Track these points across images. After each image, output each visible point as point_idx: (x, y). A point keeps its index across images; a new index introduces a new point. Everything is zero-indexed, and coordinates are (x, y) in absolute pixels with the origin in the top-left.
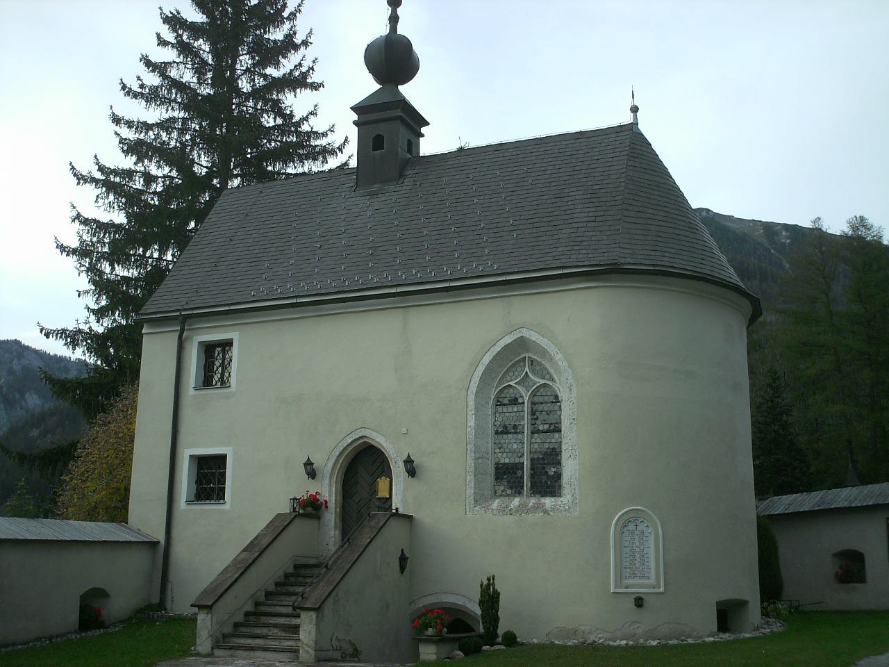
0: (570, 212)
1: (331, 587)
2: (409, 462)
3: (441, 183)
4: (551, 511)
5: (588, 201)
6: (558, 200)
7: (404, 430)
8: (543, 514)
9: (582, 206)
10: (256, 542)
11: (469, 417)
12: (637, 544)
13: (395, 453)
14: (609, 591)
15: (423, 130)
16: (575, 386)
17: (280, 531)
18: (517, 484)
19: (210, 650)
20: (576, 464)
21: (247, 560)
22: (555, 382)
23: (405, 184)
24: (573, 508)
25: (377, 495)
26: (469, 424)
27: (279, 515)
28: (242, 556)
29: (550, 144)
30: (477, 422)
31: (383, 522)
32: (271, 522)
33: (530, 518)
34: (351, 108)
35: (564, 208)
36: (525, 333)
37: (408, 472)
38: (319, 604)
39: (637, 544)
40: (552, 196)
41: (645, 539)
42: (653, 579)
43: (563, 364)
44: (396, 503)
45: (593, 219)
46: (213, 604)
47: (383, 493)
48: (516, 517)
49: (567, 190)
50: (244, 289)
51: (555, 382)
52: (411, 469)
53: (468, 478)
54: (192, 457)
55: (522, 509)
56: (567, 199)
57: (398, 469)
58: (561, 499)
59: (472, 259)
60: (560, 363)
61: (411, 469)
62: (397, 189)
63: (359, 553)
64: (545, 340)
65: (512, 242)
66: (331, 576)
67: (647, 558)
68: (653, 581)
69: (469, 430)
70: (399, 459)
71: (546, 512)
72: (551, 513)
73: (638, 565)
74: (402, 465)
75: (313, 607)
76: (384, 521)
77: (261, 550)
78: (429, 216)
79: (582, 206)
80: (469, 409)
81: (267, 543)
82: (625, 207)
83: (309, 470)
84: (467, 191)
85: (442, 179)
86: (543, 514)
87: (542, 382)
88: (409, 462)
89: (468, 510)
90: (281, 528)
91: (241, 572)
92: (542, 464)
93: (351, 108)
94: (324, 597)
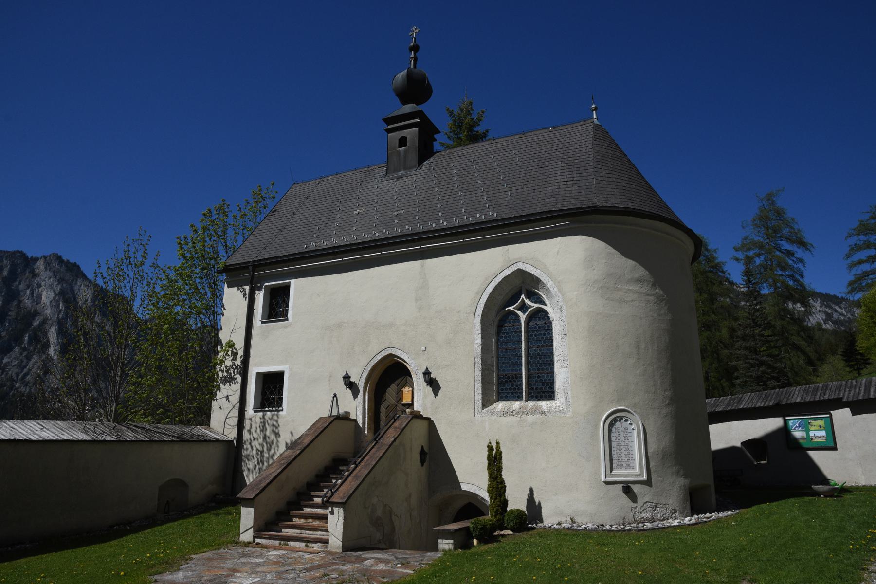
0: (552, 176)
1: (358, 482)
2: (427, 373)
3: (450, 167)
4: (548, 412)
5: (566, 168)
6: (541, 169)
7: (423, 348)
8: (540, 415)
9: (561, 171)
10: (300, 441)
11: (476, 335)
12: (623, 439)
13: (415, 367)
14: (601, 480)
15: (435, 136)
16: (564, 307)
17: (320, 431)
18: (535, 390)
19: (251, 539)
20: (568, 372)
21: (290, 457)
22: (546, 305)
23: (423, 169)
24: (567, 409)
25: (402, 401)
26: (476, 342)
27: (321, 418)
28: (286, 453)
29: (532, 136)
30: (483, 340)
31: (405, 424)
32: (314, 424)
33: (530, 419)
34: (383, 119)
35: (547, 174)
36: (521, 266)
37: (427, 382)
38: (347, 498)
39: (623, 439)
40: (536, 167)
41: (629, 434)
42: (637, 469)
43: (554, 290)
44: (417, 407)
45: (571, 179)
46: (255, 497)
47: (407, 400)
48: (518, 418)
49: (548, 163)
50: (280, 223)
51: (546, 305)
52: (433, 383)
53: (476, 386)
54: (258, 374)
55: (521, 412)
56: (548, 168)
57: (418, 380)
58: (555, 402)
59: (476, 212)
60: (551, 289)
61: (433, 383)
62: (416, 173)
63: (384, 451)
64: (538, 271)
65: (508, 198)
66: (360, 471)
67: (631, 451)
68: (637, 470)
69: (476, 346)
70: (419, 371)
71: (543, 413)
72: (548, 414)
73: (624, 457)
74: (421, 377)
75: (340, 501)
76: (407, 422)
77: (302, 448)
78: (441, 187)
79: (561, 171)
80: (476, 329)
81: (309, 442)
82: (596, 170)
83: (347, 382)
84: (470, 170)
85: (450, 164)
86: (540, 415)
87: (535, 305)
88: (427, 373)
89: (476, 413)
90: (322, 429)
91: (283, 467)
92: (538, 374)
93: (383, 119)
94: (351, 492)
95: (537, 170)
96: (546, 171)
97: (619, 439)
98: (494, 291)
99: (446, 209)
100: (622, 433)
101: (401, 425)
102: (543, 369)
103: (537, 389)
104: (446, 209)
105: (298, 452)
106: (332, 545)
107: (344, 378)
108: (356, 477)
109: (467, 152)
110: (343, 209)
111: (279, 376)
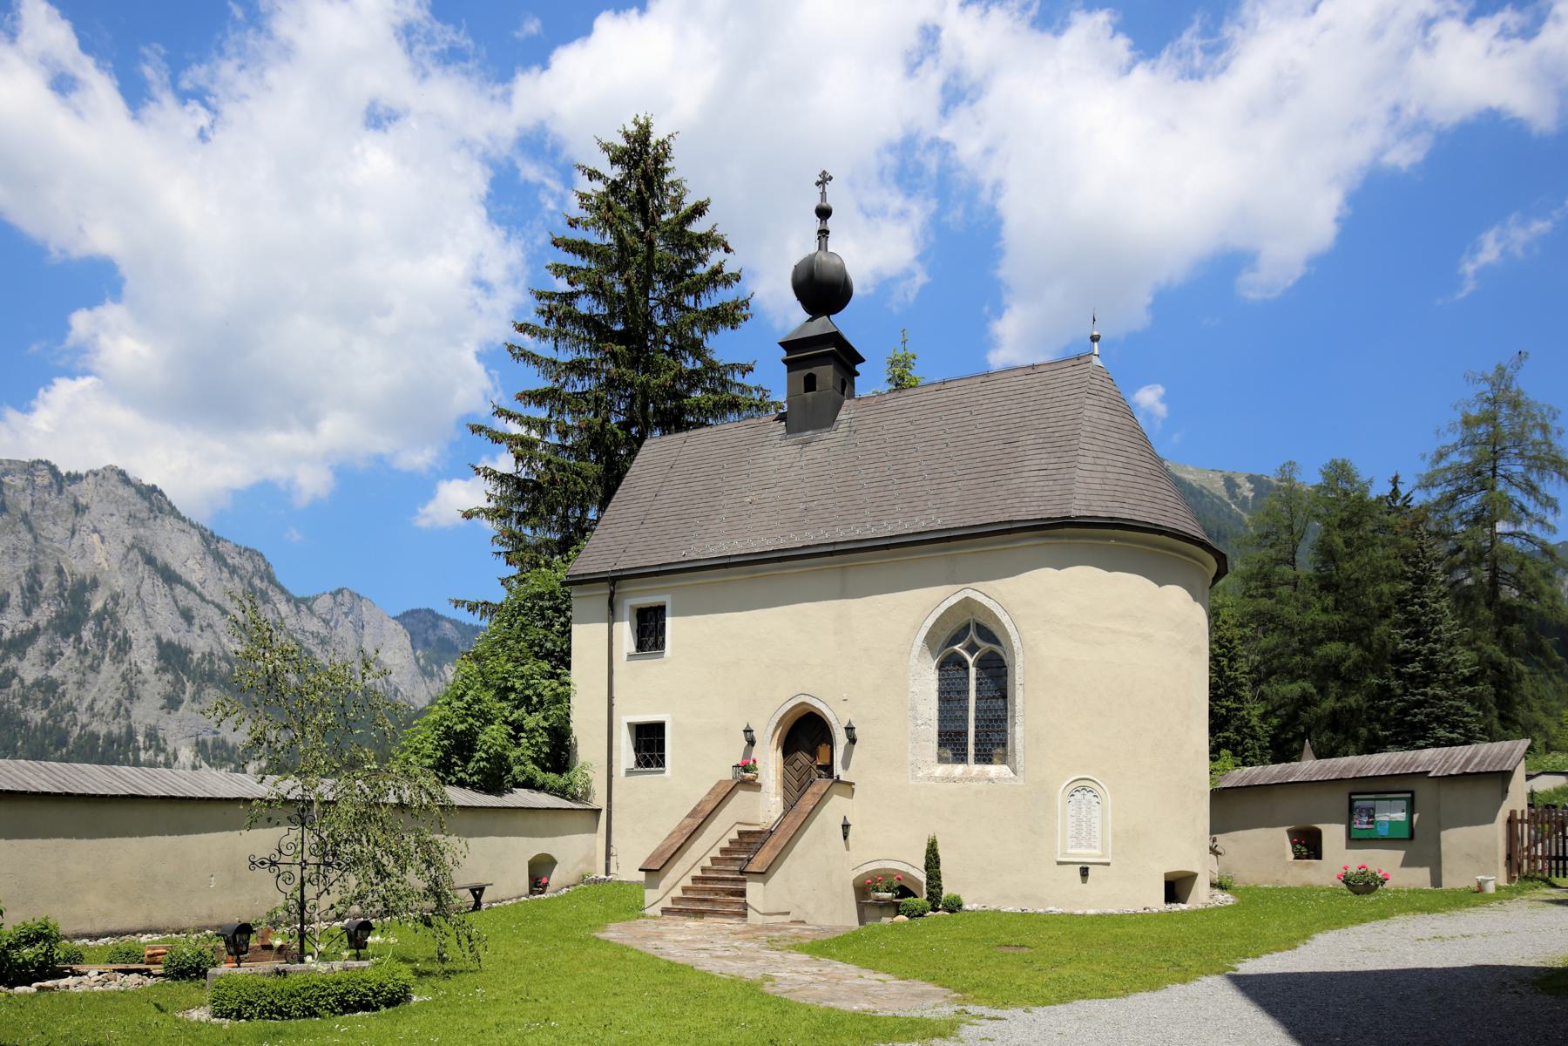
1: (777, 852)
27: (720, 782)
32: (713, 789)
39: (1085, 814)
95: (1002, 447)
96: (1014, 450)
97: (1080, 813)
98: (934, 625)
99: (875, 504)
100: (1083, 806)
101: (820, 790)
102: (993, 726)
103: (985, 750)
104: (875, 504)
105: (701, 820)
106: (1296, 486)
107: (745, 731)
108: (774, 846)
109: (904, 402)
110: (729, 492)
111: (658, 728)
